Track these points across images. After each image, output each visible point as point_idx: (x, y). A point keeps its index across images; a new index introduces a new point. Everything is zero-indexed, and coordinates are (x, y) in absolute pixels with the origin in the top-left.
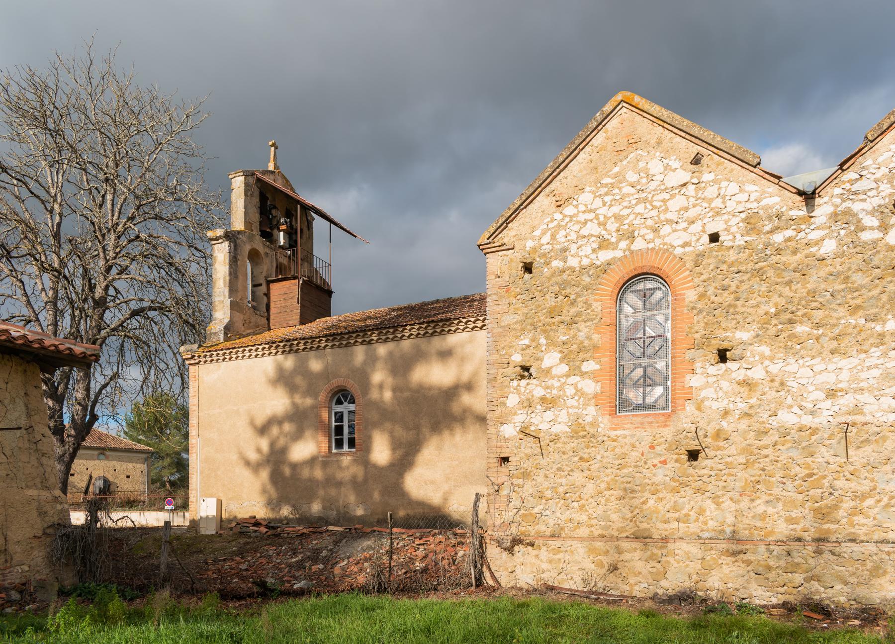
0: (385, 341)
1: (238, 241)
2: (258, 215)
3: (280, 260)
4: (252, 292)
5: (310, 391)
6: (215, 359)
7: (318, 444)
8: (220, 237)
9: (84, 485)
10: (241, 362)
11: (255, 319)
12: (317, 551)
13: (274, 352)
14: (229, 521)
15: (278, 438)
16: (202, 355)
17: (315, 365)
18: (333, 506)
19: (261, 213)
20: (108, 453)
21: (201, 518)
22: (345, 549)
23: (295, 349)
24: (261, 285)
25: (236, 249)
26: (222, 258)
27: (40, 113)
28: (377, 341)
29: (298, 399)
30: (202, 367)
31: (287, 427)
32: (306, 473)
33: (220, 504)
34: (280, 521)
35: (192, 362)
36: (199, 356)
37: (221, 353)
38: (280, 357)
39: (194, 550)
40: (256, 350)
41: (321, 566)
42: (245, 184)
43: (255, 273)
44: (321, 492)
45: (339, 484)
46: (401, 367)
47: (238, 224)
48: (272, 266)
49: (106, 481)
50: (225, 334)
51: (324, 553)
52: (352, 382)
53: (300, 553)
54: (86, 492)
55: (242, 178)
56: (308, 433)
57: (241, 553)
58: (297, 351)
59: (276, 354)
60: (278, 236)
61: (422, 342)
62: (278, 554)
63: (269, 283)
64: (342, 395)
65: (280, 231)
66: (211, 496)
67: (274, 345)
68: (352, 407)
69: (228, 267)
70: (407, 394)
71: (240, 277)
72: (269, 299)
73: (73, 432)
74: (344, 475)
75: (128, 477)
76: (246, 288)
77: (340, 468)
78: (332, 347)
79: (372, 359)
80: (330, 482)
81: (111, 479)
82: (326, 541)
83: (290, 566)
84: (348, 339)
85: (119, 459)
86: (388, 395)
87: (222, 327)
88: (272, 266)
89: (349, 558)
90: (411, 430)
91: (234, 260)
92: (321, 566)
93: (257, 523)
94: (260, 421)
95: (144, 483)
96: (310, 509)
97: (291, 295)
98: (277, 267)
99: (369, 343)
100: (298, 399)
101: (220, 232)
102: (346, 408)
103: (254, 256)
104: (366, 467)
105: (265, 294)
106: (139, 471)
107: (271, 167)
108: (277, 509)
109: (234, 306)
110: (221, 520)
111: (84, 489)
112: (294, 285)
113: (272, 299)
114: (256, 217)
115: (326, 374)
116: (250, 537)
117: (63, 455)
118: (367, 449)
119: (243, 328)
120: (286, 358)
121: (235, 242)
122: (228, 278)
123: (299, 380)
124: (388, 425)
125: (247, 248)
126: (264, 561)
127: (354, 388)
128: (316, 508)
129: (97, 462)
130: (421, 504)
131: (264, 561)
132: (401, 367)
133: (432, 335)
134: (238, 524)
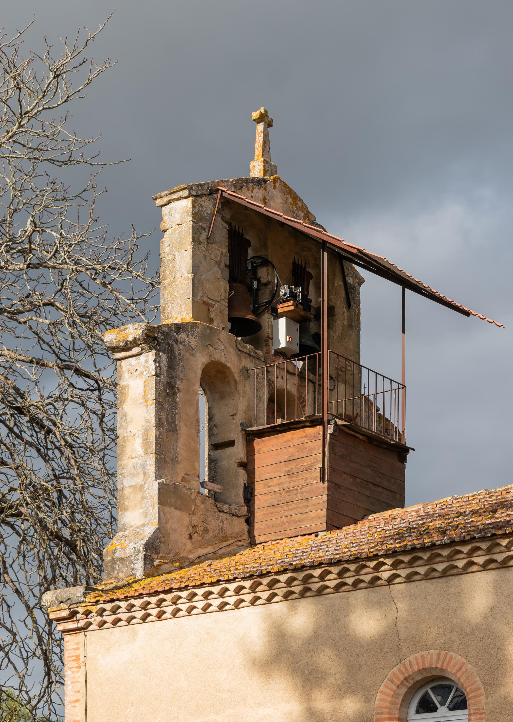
1: (178, 348)
2: (224, 285)
3: (280, 383)
4: (212, 461)
8: (135, 343)
16: (95, 609)
17: (366, 621)
19: (232, 280)
23: (315, 587)
24: (231, 443)
25: (171, 366)
26: (141, 390)
30: (94, 635)
35: (71, 625)
36: (87, 613)
37: (138, 603)
38: (279, 607)
40: (221, 594)
43: (217, 419)
47: (177, 306)
48: (258, 399)
50: (148, 560)
52: (457, 658)
55: (188, 203)
58: (320, 592)
59: (269, 600)
60: (275, 329)
63: (250, 437)
65: (277, 316)
67: (265, 581)
71: (183, 430)
76: (196, 453)
78: (409, 579)
84: (450, 558)
88: (258, 399)
91: (167, 392)
97: (306, 463)
98: (271, 400)
101: (133, 331)
103: (215, 379)
105: (243, 465)
107: (256, 170)
109: (168, 496)
113: (259, 474)
114: (219, 289)
115: (391, 643)
119: (189, 546)
120: (292, 609)
122: (153, 434)
123: (326, 659)
125: (200, 361)
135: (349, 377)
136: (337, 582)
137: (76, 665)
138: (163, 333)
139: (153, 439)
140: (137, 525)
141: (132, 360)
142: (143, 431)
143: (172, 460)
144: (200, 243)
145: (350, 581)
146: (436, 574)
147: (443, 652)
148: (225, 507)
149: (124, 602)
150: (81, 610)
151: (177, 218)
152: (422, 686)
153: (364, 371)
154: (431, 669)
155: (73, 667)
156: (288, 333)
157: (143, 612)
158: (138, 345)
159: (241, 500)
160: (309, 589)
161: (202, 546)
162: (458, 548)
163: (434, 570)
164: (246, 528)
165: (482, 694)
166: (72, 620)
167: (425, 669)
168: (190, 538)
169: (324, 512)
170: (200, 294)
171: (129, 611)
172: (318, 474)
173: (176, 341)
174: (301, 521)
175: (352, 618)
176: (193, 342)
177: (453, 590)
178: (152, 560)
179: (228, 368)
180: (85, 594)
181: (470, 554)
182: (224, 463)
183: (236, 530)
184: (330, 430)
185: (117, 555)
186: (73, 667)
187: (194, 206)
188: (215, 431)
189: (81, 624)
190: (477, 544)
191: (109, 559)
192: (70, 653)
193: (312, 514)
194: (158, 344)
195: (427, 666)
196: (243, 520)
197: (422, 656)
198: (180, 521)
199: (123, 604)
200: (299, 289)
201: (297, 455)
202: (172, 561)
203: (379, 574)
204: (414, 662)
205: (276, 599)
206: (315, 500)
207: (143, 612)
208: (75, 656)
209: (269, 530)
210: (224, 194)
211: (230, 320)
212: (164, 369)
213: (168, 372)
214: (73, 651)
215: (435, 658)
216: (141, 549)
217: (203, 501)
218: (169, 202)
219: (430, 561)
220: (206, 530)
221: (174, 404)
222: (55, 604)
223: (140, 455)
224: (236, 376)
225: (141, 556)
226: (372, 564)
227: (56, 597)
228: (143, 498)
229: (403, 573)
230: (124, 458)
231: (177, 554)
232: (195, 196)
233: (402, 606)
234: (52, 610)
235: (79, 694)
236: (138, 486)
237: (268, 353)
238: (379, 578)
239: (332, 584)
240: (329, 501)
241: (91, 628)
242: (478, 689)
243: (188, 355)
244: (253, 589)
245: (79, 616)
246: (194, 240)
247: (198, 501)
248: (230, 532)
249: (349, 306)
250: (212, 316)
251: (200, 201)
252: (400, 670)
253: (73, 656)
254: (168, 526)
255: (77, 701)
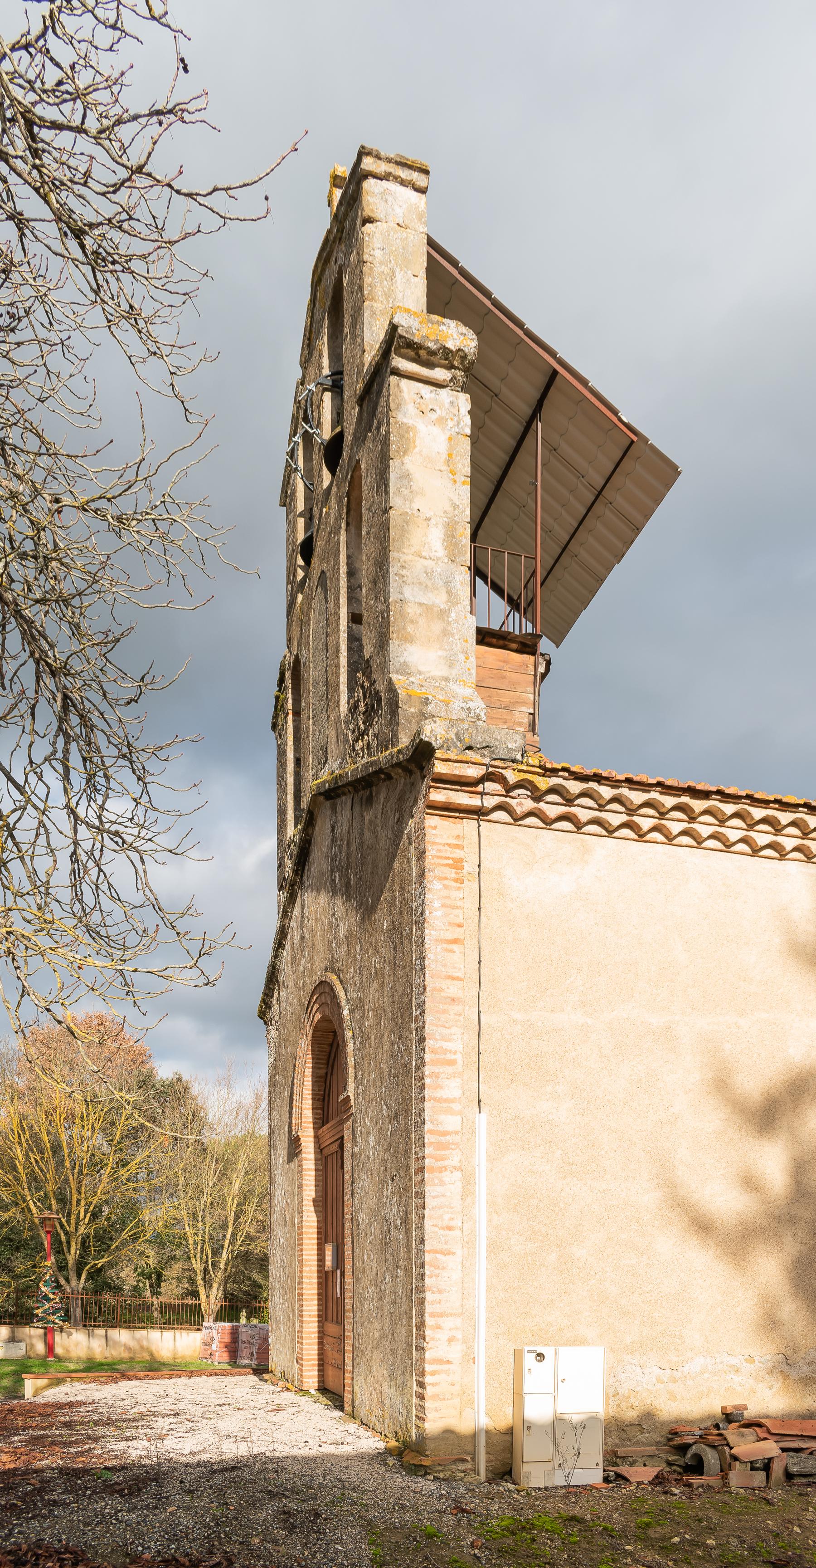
137: (454, 875)
140: (432, 674)
141: (425, 389)
142: (445, 519)
149: (609, 788)
155: (446, 878)
158: (450, 367)
166: (473, 789)
186: (446, 878)
191: (413, 710)
192: (440, 851)
208: (453, 859)
214: (447, 847)
222: (456, 747)
223: (438, 559)
227: (457, 735)
228: (446, 633)
230: (405, 551)
234: (445, 756)
235: (461, 930)
236: (436, 609)
253: (448, 858)
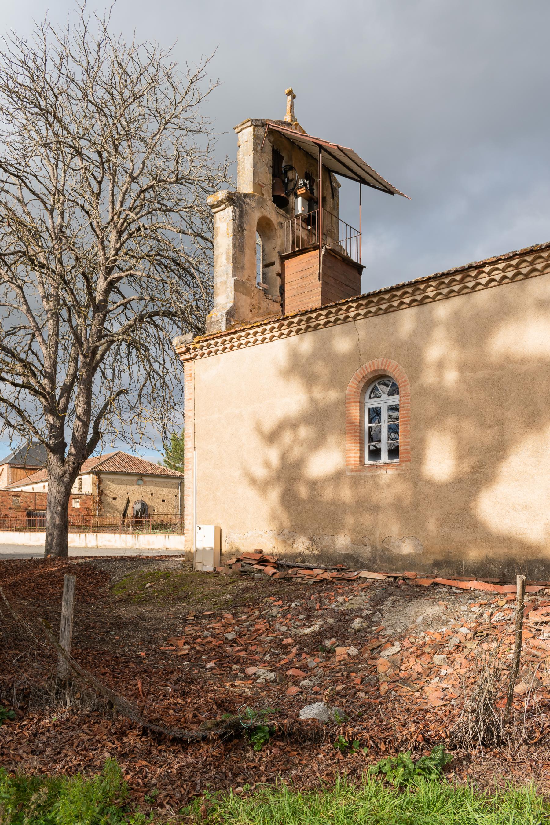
0: (447, 297)
1: (244, 206)
2: (270, 176)
3: (298, 233)
4: (264, 274)
5: (335, 381)
6: (213, 350)
7: (345, 452)
8: (222, 202)
9: (122, 508)
10: (244, 351)
11: (265, 304)
12: (344, 617)
13: (286, 332)
14: (231, 555)
15: (291, 447)
16: (198, 346)
17: (342, 343)
18: (366, 540)
19: (274, 175)
20: (145, 479)
21: (197, 550)
22: (395, 618)
23: (313, 325)
24: (273, 263)
25: (241, 216)
26: (225, 229)
27: (39, 101)
28: (434, 299)
29: (318, 394)
30: (199, 362)
31: (304, 432)
32: (328, 493)
33: (219, 533)
34: (294, 557)
35: (187, 356)
36: (195, 349)
37: (220, 340)
38: (294, 339)
39: (180, 594)
40: (263, 333)
41: (353, 650)
42: (255, 136)
43: (267, 250)
44: (349, 520)
45: (376, 509)
46: (473, 333)
47: (246, 185)
48: (287, 240)
49: (144, 505)
50: (228, 321)
51: (357, 623)
52: (394, 363)
53: (318, 617)
54: (125, 515)
55: (251, 129)
56: (332, 439)
57: (235, 606)
58: (316, 328)
59: (288, 335)
60: (295, 204)
61: (508, 289)
62: (284, 616)
63: (284, 258)
64: (379, 381)
65: (297, 196)
66: (209, 523)
67: (286, 323)
68: (394, 400)
69: (231, 238)
70: (482, 373)
71: (248, 252)
72: (283, 280)
73: (73, 451)
74: (386, 497)
75: (163, 501)
76: (254, 265)
77: (377, 486)
78: (366, 316)
79: (426, 328)
80: (362, 505)
81: (148, 503)
82: (360, 600)
83: (300, 641)
84: (390, 300)
85: (156, 485)
86: (451, 377)
87: (224, 313)
88: (287, 240)
89: (401, 638)
90: (490, 427)
91: (239, 230)
92: (353, 650)
93: (263, 561)
94: (268, 426)
95: (177, 507)
96: (334, 543)
97: (311, 271)
98: (293, 243)
99: (422, 303)
100: (318, 394)
101: (221, 195)
102: (384, 402)
103: (265, 227)
104: (416, 484)
105: (279, 275)
106: (173, 496)
107: (288, 119)
108: (290, 542)
109: (239, 286)
110: (221, 554)
111: (122, 513)
112: (314, 257)
113: (288, 279)
114: (267, 178)
115: (356, 356)
116: (253, 579)
117: (63, 475)
118: (419, 459)
119: (250, 315)
120: (301, 339)
121: (241, 207)
122: (231, 252)
123: (320, 367)
124: (451, 422)
125: (256, 215)
126: (261, 625)
127: (396, 369)
128: (342, 542)
129: (136, 487)
130: (506, 540)
131: (261, 625)
132: (473, 333)
133: (527, 276)
134: (239, 560)
135: (333, 235)
136: (325, 320)
138: (237, 197)
139: (231, 255)
143: (242, 268)
144: (257, 151)
145: (332, 320)
146: (381, 312)
147: (385, 360)
148: (270, 297)
150: (191, 347)
151: (246, 138)
152: (373, 382)
153: (341, 222)
154: (378, 370)
156: (302, 206)
157: (223, 346)
159: (278, 293)
160: (310, 327)
161: (257, 316)
162: (394, 293)
163: (381, 309)
164: (280, 309)
165: (408, 384)
167: (374, 370)
168: (251, 311)
169: (320, 297)
170: (257, 179)
171: (216, 346)
172: (317, 276)
173: (244, 202)
174: (308, 303)
175: (334, 342)
176: (253, 204)
177: (391, 321)
178: (230, 321)
179: (272, 221)
180: (194, 338)
181: (402, 296)
182: (270, 274)
183: (276, 309)
184: (323, 252)
185: (213, 319)
187: (254, 131)
188: (266, 257)
189: (192, 355)
190: (406, 290)
193: (314, 299)
194: (234, 202)
195: (376, 368)
196: (279, 304)
197: (373, 363)
198: (245, 302)
199: (212, 342)
200: (308, 182)
201: (306, 267)
202: (241, 323)
203: (348, 314)
204: (368, 366)
205: (292, 334)
206: (315, 291)
207: (223, 346)
209: (292, 309)
210: (270, 127)
211: (273, 196)
212: (238, 217)
213: (239, 219)
215: (380, 363)
216: (225, 315)
217: (258, 292)
218: (242, 130)
219: (378, 303)
220: (260, 308)
221: (243, 237)
224: (276, 226)
225: (225, 319)
226: (345, 307)
228: (227, 288)
229: (362, 312)
231: (244, 319)
232: (255, 126)
233: (362, 333)
237: (292, 217)
238: (348, 317)
239: (322, 322)
240: (322, 291)
241: (197, 357)
242: (406, 381)
243: (250, 211)
244: (280, 328)
245: (191, 351)
246: (254, 149)
247: (255, 291)
248: (272, 310)
249: (333, 198)
250: (264, 192)
251: (257, 128)
252: (360, 372)
254: (239, 304)
255: (190, 399)
